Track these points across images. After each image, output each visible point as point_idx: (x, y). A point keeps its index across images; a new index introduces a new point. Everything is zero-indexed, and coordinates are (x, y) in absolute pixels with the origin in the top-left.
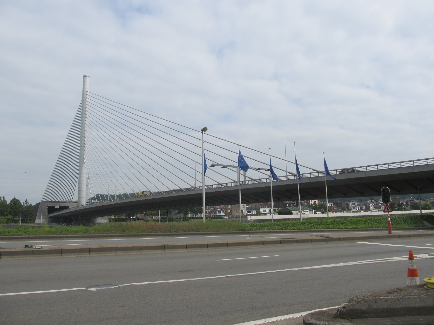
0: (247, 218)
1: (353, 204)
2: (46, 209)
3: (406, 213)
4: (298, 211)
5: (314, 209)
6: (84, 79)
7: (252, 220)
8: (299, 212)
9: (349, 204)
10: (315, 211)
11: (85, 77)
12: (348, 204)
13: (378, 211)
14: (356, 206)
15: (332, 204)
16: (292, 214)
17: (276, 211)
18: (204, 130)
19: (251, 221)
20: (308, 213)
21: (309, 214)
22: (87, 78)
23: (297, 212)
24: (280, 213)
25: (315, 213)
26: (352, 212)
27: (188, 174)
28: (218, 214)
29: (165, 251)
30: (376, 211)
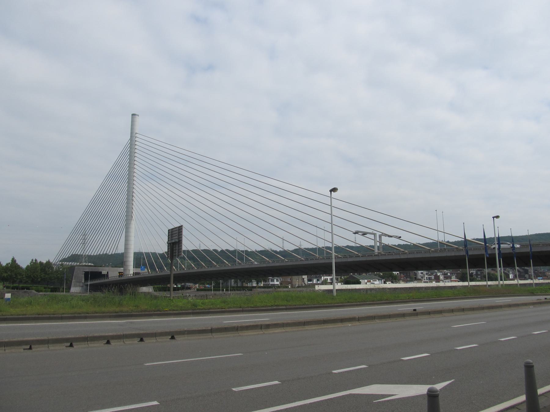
2: (82, 274)
4: (366, 281)
5: (383, 278)
6: (132, 118)
7: (320, 290)
8: (368, 281)
9: (416, 273)
11: (133, 116)
12: (416, 273)
13: (450, 282)
14: (424, 275)
15: (398, 272)
16: (360, 284)
17: (339, 280)
18: (334, 190)
20: (377, 282)
21: (378, 284)
22: (137, 116)
23: (365, 282)
24: (347, 282)
25: (385, 283)
26: (424, 282)
28: (271, 283)
30: (448, 282)
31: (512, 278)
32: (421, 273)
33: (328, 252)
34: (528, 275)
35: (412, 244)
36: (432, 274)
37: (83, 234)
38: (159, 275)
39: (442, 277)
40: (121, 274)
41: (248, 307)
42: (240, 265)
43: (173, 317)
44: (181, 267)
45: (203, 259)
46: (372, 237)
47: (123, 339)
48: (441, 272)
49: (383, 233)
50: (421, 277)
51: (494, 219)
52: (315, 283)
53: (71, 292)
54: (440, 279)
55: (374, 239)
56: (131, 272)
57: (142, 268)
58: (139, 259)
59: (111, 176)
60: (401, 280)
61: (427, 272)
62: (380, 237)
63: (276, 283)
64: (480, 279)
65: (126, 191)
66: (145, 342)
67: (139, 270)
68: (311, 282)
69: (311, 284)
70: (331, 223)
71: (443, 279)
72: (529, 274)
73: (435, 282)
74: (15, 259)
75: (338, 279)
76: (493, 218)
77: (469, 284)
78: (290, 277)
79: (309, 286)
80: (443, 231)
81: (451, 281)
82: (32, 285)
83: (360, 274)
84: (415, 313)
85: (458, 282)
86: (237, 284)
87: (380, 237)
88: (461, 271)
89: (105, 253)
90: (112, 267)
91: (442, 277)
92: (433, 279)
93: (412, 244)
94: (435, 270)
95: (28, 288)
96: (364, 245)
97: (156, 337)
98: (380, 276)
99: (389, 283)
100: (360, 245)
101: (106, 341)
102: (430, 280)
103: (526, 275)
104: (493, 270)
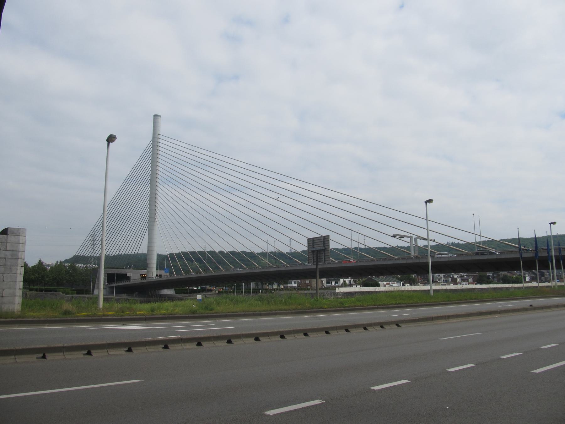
0: (335, 289)
1: (438, 275)
3: (498, 287)
4: (385, 283)
6: (154, 119)
7: (340, 292)
8: (387, 284)
10: (403, 283)
11: (156, 117)
15: (416, 275)
16: (379, 286)
19: (340, 294)
20: (396, 285)
21: (396, 286)
24: (365, 285)
25: (403, 285)
27: (384, 233)
29: (64, 355)
31: (529, 280)
32: (439, 276)
33: (362, 254)
34: (544, 278)
35: (391, 247)
36: (449, 276)
37: (92, 235)
38: (175, 278)
39: (459, 280)
40: (143, 277)
41: (396, 304)
42: (258, 268)
43: (227, 319)
44: (208, 269)
45: (220, 262)
46: (408, 240)
47: (15, 356)
48: (457, 275)
49: (418, 236)
50: (438, 280)
51: (550, 225)
52: (333, 285)
53: (94, 294)
54: (457, 282)
55: (410, 242)
56: (155, 275)
57: (166, 270)
58: (163, 261)
59: (130, 180)
60: (419, 282)
61: (444, 275)
62: (416, 240)
63: (294, 285)
64: (496, 282)
65: (148, 195)
66: (92, 356)
67: (160, 272)
68: (330, 285)
69: (330, 286)
70: (426, 228)
71: (460, 282)
72: (545, 276)
73: (453, 285)
74: (27, 263)
75: (356, 282)
76: (550, 224)
77: (538, 284)
78: (310, 280)
79: (328, 288)
80: (480, 235)
81: (469, 284)
82: (57, 287)
83: (378, 277)
84: (532, 308)
85: (476, 284)
86: (258, 287)
87: (416, 240)
88: (477, 274)
89: (108, 254)
90: (133, 269)
91: (459, 280)
92: (450, 282)
93: (391, 247)
94: (514, 271)
95: (55, 291)
96: (372, 247)
97: (389, 324)
98: (398, 278)
99: (408, 286)
100: (390, 246)
101: (163, 346)
102: (448, 283)
103: (542, 278)
104: (509, 272)
